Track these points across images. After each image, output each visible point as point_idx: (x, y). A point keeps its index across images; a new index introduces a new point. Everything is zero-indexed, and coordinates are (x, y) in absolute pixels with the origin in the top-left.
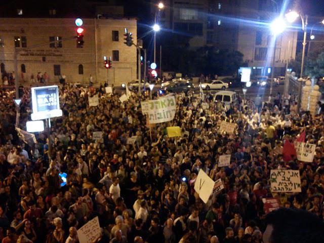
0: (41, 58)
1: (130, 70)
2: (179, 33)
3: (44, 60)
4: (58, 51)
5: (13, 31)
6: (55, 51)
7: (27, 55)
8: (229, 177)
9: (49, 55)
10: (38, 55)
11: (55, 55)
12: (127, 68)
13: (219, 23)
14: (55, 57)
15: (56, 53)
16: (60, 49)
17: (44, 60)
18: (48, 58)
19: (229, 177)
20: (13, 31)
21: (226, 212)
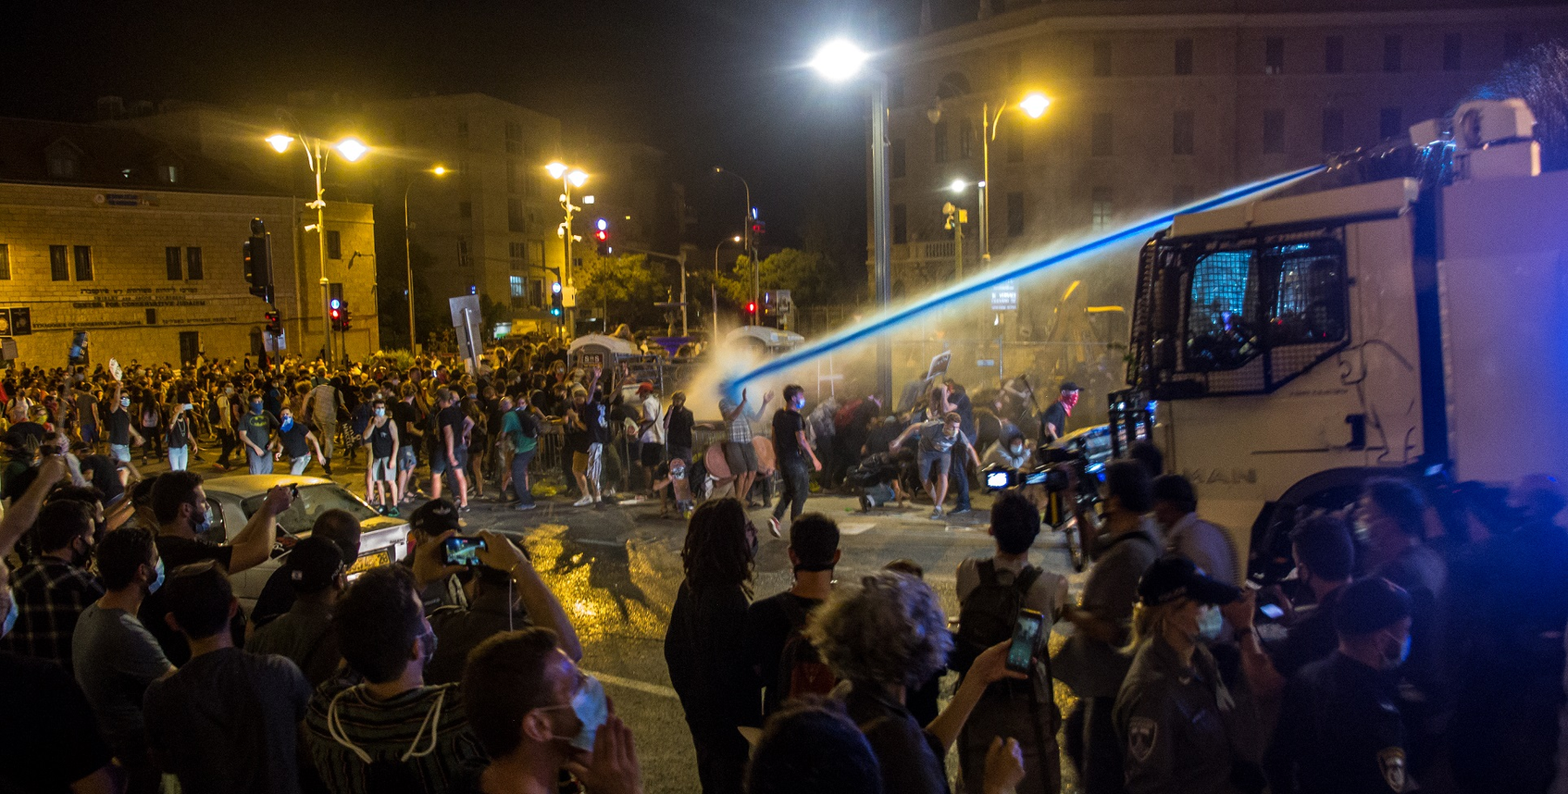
0: (140, 315)
1: (363, 335)
2: (479, 648)
3: (151, 318)
4: (193, 291)
5: (464, 249)
6: (183, 290)
7: (96, 305)
8: (1400, 144)
9: (160, 304)
10: (133, 304)
11: (185, 304)
12: (1427, 303)
13: (737, 239)
14: (183, 309)
15: (189, 297)
16: (198, 284)
17: (151, 318)
18: (163, 313)
19: (1400, 144)
20: (464, 249)
21: (439, 363)
